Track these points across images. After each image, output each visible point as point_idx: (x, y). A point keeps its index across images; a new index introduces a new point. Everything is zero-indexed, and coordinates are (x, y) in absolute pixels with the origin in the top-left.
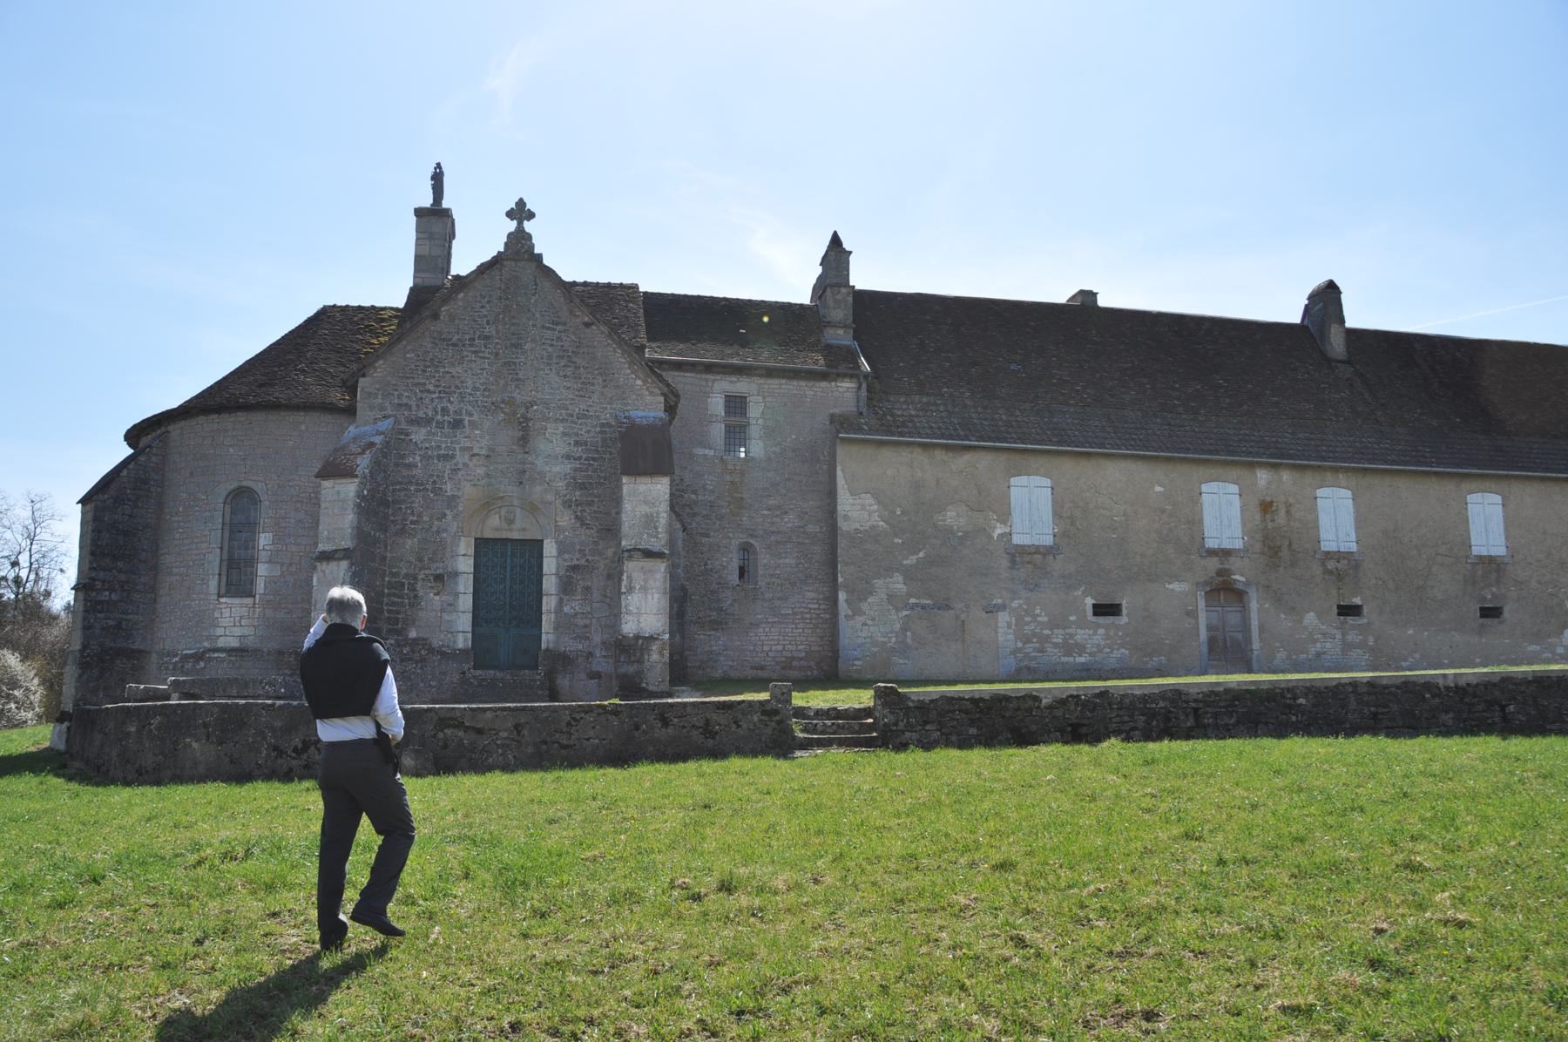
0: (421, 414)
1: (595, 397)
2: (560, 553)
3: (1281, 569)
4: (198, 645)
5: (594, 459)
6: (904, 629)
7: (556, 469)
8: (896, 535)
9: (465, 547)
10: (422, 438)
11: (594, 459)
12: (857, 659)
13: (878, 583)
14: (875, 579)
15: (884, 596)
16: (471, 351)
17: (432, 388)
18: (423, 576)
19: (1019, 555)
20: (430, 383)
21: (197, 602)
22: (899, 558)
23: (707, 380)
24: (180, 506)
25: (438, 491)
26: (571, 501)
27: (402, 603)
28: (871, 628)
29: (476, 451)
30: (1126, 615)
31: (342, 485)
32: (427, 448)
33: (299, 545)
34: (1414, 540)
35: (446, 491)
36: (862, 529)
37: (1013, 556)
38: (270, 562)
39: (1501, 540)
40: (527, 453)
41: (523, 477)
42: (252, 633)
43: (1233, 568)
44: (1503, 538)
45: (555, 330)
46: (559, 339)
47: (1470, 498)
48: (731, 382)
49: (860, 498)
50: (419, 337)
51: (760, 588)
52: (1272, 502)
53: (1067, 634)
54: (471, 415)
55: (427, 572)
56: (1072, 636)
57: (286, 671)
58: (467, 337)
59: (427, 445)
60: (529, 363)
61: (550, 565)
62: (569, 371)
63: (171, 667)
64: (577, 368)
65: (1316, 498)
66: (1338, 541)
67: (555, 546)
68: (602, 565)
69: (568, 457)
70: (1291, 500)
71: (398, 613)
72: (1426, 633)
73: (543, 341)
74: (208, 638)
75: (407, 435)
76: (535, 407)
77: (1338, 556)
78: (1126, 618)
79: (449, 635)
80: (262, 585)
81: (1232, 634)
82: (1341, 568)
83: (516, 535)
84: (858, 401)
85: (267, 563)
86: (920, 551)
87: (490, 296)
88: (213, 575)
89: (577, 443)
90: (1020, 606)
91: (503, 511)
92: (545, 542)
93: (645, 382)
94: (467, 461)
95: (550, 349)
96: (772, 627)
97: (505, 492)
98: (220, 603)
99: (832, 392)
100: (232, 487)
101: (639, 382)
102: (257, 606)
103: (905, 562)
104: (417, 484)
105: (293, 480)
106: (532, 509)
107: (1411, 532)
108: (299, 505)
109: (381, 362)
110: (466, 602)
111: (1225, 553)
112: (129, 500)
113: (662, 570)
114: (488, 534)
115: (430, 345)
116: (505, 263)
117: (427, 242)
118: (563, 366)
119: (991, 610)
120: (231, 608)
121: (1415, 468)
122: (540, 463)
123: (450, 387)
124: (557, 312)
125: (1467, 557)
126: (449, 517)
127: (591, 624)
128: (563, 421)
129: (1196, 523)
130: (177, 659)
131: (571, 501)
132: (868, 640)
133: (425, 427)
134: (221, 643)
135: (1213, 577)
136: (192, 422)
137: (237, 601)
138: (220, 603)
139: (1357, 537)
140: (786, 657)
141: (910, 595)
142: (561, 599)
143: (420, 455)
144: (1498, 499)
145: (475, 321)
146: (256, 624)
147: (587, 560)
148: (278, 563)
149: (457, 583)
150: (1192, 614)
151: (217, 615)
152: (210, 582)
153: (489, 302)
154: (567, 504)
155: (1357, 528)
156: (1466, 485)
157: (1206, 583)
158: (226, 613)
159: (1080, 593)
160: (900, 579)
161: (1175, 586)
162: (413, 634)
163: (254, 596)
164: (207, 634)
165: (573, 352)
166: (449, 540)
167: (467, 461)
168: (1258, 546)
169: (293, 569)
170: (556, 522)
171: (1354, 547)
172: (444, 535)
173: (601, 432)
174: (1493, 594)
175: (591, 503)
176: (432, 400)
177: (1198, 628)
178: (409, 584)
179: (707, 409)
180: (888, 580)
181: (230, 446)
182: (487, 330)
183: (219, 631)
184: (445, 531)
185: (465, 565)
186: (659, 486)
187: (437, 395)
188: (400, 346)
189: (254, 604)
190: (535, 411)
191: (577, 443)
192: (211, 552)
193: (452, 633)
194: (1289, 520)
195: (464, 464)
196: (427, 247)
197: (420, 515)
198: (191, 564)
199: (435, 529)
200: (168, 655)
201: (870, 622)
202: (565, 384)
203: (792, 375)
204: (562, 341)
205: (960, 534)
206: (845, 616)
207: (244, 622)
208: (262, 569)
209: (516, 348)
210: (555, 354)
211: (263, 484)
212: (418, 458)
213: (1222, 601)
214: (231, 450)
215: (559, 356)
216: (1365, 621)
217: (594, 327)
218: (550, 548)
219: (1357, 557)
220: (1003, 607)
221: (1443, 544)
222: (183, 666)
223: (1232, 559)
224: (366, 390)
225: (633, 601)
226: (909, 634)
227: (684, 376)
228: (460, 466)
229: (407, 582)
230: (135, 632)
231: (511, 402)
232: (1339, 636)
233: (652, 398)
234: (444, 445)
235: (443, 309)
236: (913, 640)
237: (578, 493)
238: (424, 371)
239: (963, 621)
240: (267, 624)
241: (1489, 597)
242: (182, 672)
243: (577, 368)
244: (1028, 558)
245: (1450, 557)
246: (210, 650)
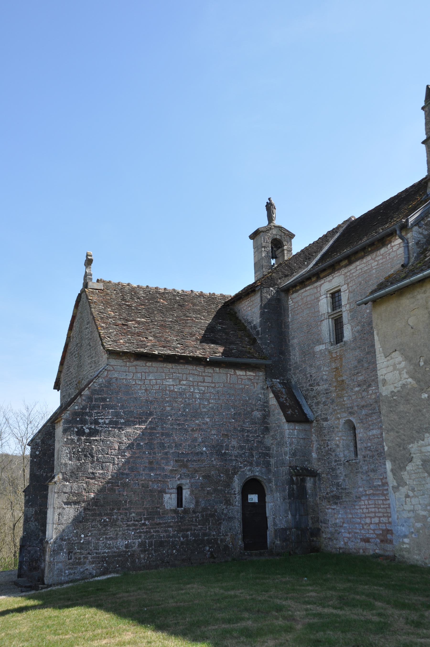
12: (405, 536)
13: (413, 447)
14: (409, 444)
15: (419, 462)
23: (316, 287)
28: (413, 500)
36: (396, 391)
48: (329, 281)
49: (392, 358)
51: (359, 462)
96: (369, 499)
99: (389, 254)
121: (421, 275)
132: (411, 514)
140: (383, 530)
179: (319, 311)
180: (421, 442)
203: (346, 262)
206: (393, 487)
219: (96, 497)
227: (306, 291)
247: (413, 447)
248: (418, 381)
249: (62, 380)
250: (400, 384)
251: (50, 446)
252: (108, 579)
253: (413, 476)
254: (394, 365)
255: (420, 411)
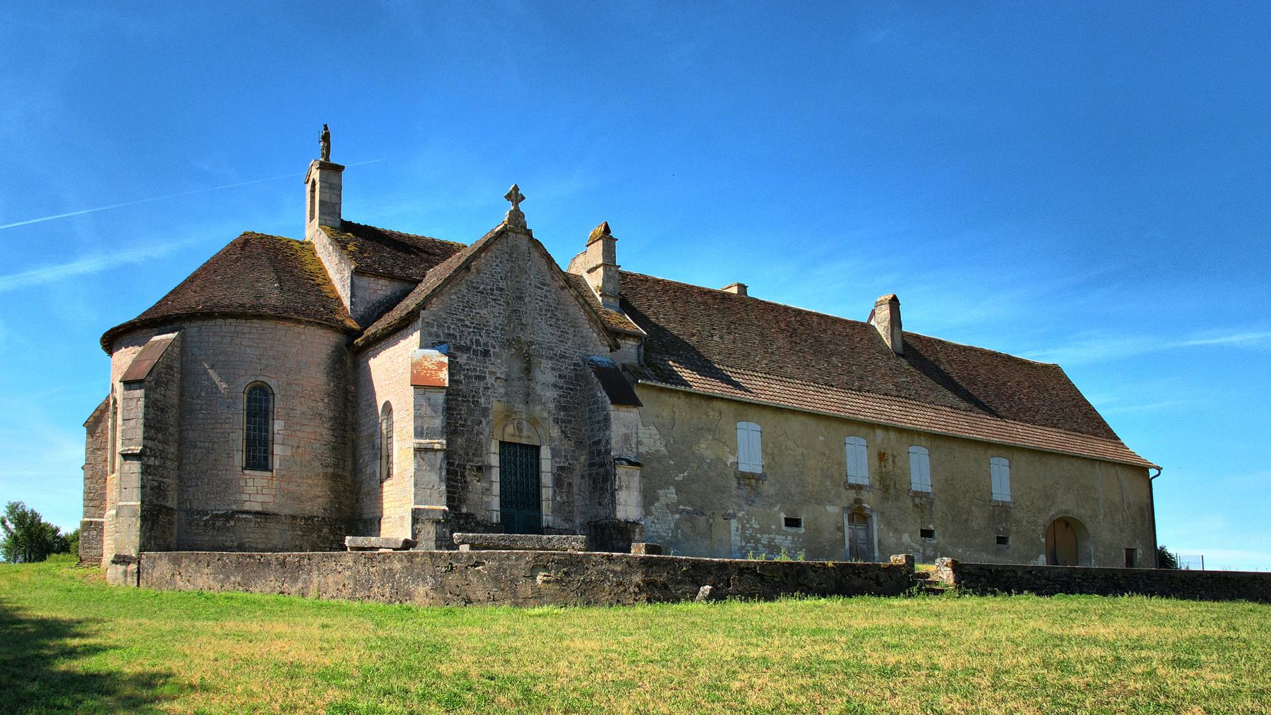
0: (462, 343)
1: (570, 343)
2: (553, 456)
3: (890, 501)
4: (227, 507)
5: (571, 389)
6: (677, 527)
7: (548, 394)
8: (670, 458)
9: (494, 447)
10: (465, 361)
11: (571, 389)
13: (661, 492)
14: (658, 489)
16: (492, 299)
17: (469, 324)
18: (470, 467)
19: (744, 477)
20: (467, 320)
21: (224, 472)
22: (673, 475)
24: (201, 391)
25: (476, 403)
26: (558, 418)
27: (457, 486)
29: (499, 375)
30: (804, 527)
31: (432, 394)
32: (468, 370)
33: (304, 432)
34: (962, 487)
35: (481, 404)
36: (650, 452)
37: (739, 479)
38: (283, 444)
39: (1008, 492)
40: (530, 380)
41: (529, 398)
42: (272, 501)
43: (863, 498)
44: (1009, 490)
45: (543, 289)
46: (546, 296)
47: (992, 460)
50: (458, 284)
52: (884, 453)
53: (770, 538)
54: (494, 348)
55: (471, 464)
56: (773, 540)
57: (298, 532)
58: (489, 287)
59: (468, 367)
60: (528, 312)
61: (546, 465)
62: (553, 321)
63: (202, 524)
64: (558, 320)
65: (909, 453)
66: (921, 484)
67: (550, 451)
68: (578, 467)
69: (555, 386)
70: (895, 453)
71: (455, 493)
72: (968, 553)
73: (536, 297)
74: (235, 502)
75: (455, 358)
76: (534, 346)
77: (917, 494)
78: (347, 543)
79: (487, 513)
80: (278, 462)
81: (861, 545)
82: (922, 502)
83: (524, 441)
84: (639, 356)
85: (281, 444)
86: (685, 471)
87: (501, 258)
88: (238, 450)
89: (560, 376)
90: (743, 516)
91: (516, 422)
92: (542, 447)
93: (598, 335)
94: (493, 382)
95: (541, 303)
97: (518, 408)
98: (244, 474)
100: (250, 381)
101: (595, 335)
102: (274, 479)
103: (676, 479)
104: (463, 397)
105: (298, 379)
106: (534, 422)
107: (961, 481)
108: (303, 399)
109: (435, 299)
110: (496, 488)
111: (859, 488)
112: (163, 382)
113: (638, 475)
114: (507, 439)
115: (466, 291)
116: (509, 234)
117: (328, 191)
118: (549, 318)
119: (727, 517)
120: (254, 479)
122: (538, 388)
123: (480, 325)
124: (544, 276)
125: (990, 501)
126: (484, 423)
127: (573, 510)
128: (551, 358)
129: (842, 464)
130: (208, 518)
131: (558, 418)
133: (466, 353)
134: (247, 507)
135: (852, 504)
136: (211, 323)
137: (258, 473)
138: (244, 474)
139: (932, 482)
141: (679, 503)
142: (555, 491)
143: (464, 375)
144: (1006, 462)
145: (493, 276)
146: (274, 493)
147: (569, 464)
148: (289, 445)
149: (490, 474)
150: (841, 529)
151: (242, 483)
152: (236, 457)
153: (501, 262)
154: (556, 421)
155: (932, 476)
156: (990, 452)
157: (849, 508)
158: (250, 483)
159: (777, 509)
160: (674, 491)
161: (830, 508)
162: (464, 510)
163: (272, 471)
164: (234, 499)
165: (555, 307)
166: (484, 440)
167: (493, 382)
168: (877, 484)
169: (300, 451)
170: (550, 433)
171: (930, 490)
172: (481, 437)
173: (575, 370)
174: (1004, 528)
175: (570, 422)
176: (469, 333)
177: (844, 540)
178: (461, 472)
180: (667, 490)
181: (248, 346)
182: (502, 284)
183: (245, 497)
184: (482, 433)
185: (495, 460)
186: (632, 414)
187: (472, 330)
188: (447, 289)
189: (272, 477)
190: (534, 349)
191: (560, 376)
192: (235, 432)
193: (489, 511)
194: (894, 467)
195: (492, 384)
196: (328, 195)
197: (466, 420)
198: (216, 440)
199: (475, 432)
200: (198, 513)
201: (656, 521)
202: (551, 331)
204: (548, 299)
205: (708, 461)
207: (265, 491)
208: (278, 450)
209: (520, 300)
210: (544, 308)
211: (276, 380)
212: (462, 377)
213: (855, 521)
214: (248, 350)
215: (546, 310)
216: (935, 541)
217: (566, 290)
218: (545, 453)
219: (931, 496)
220: (734, 516)
221: (978, 491)
222: (214, 524)
223: (864, 492)
224: (426, 320)
225: (622, 496)
226: (679, 531)
228: (489, 386)
229: (459, 470)
230: (168, 493)
231: (518, 340)
232: (921, 551)
233: (602, 347)
234: (478, 369)
235: (473, 264)
236: (682, 536)
237: (562, 413)
238: (463, 310)
239: (711, 524)
240: (282, 493)
241: (1001, 529)
242: (214, 528)
243: (558, 320)
244: (747, 481)
245: (981, 500)
246: (238, 512)
247: (661, 492)
248: (669, 452)
249: (154, 370)
250: (654, 449)
251: (606, 245)
252: (43, 221)
253: (659, 511)
254: (651, 435)
255: (668, 471)
